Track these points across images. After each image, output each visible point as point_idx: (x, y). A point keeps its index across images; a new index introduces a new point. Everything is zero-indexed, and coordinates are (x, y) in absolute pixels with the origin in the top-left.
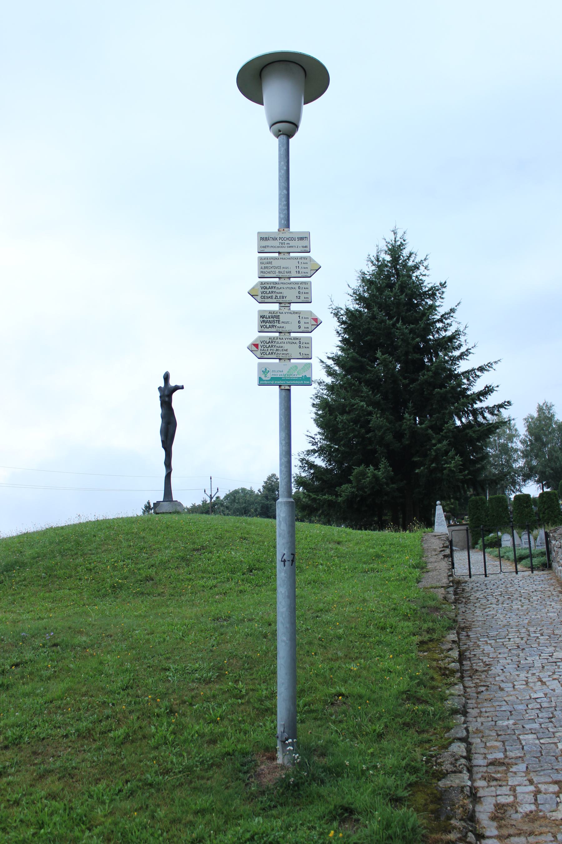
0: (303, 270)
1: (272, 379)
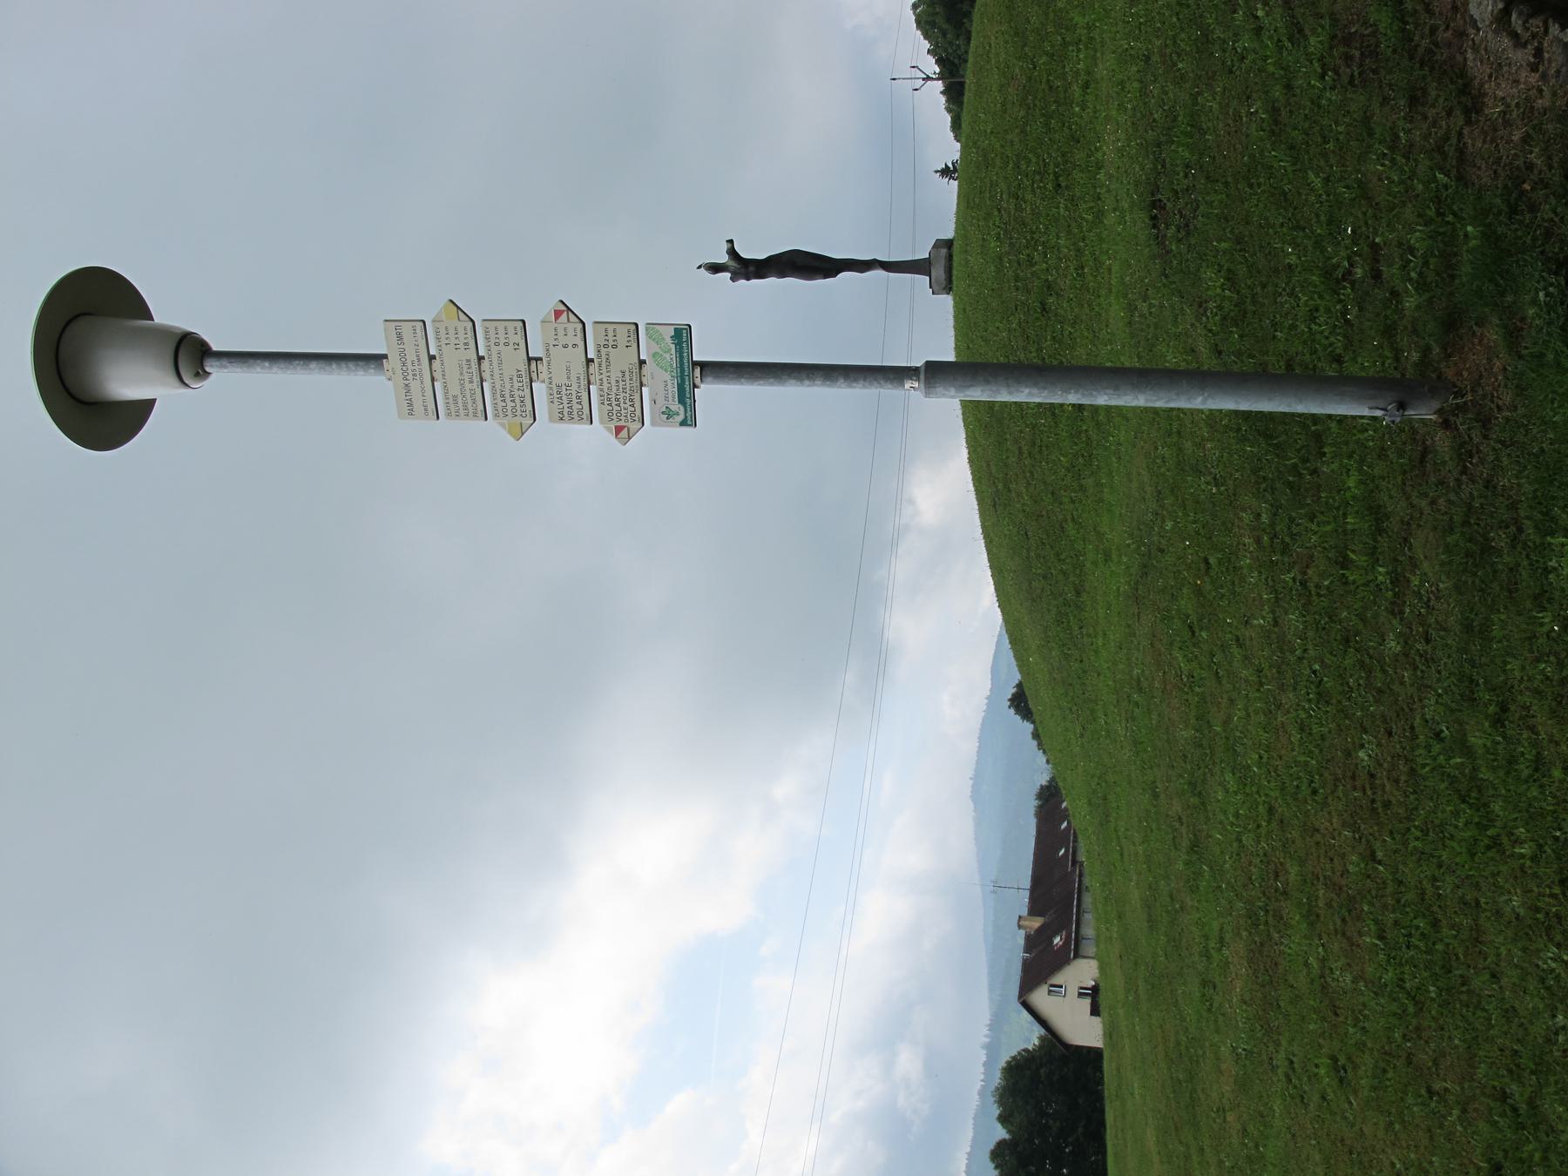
0: (461, 335)
1: (682, 401)
